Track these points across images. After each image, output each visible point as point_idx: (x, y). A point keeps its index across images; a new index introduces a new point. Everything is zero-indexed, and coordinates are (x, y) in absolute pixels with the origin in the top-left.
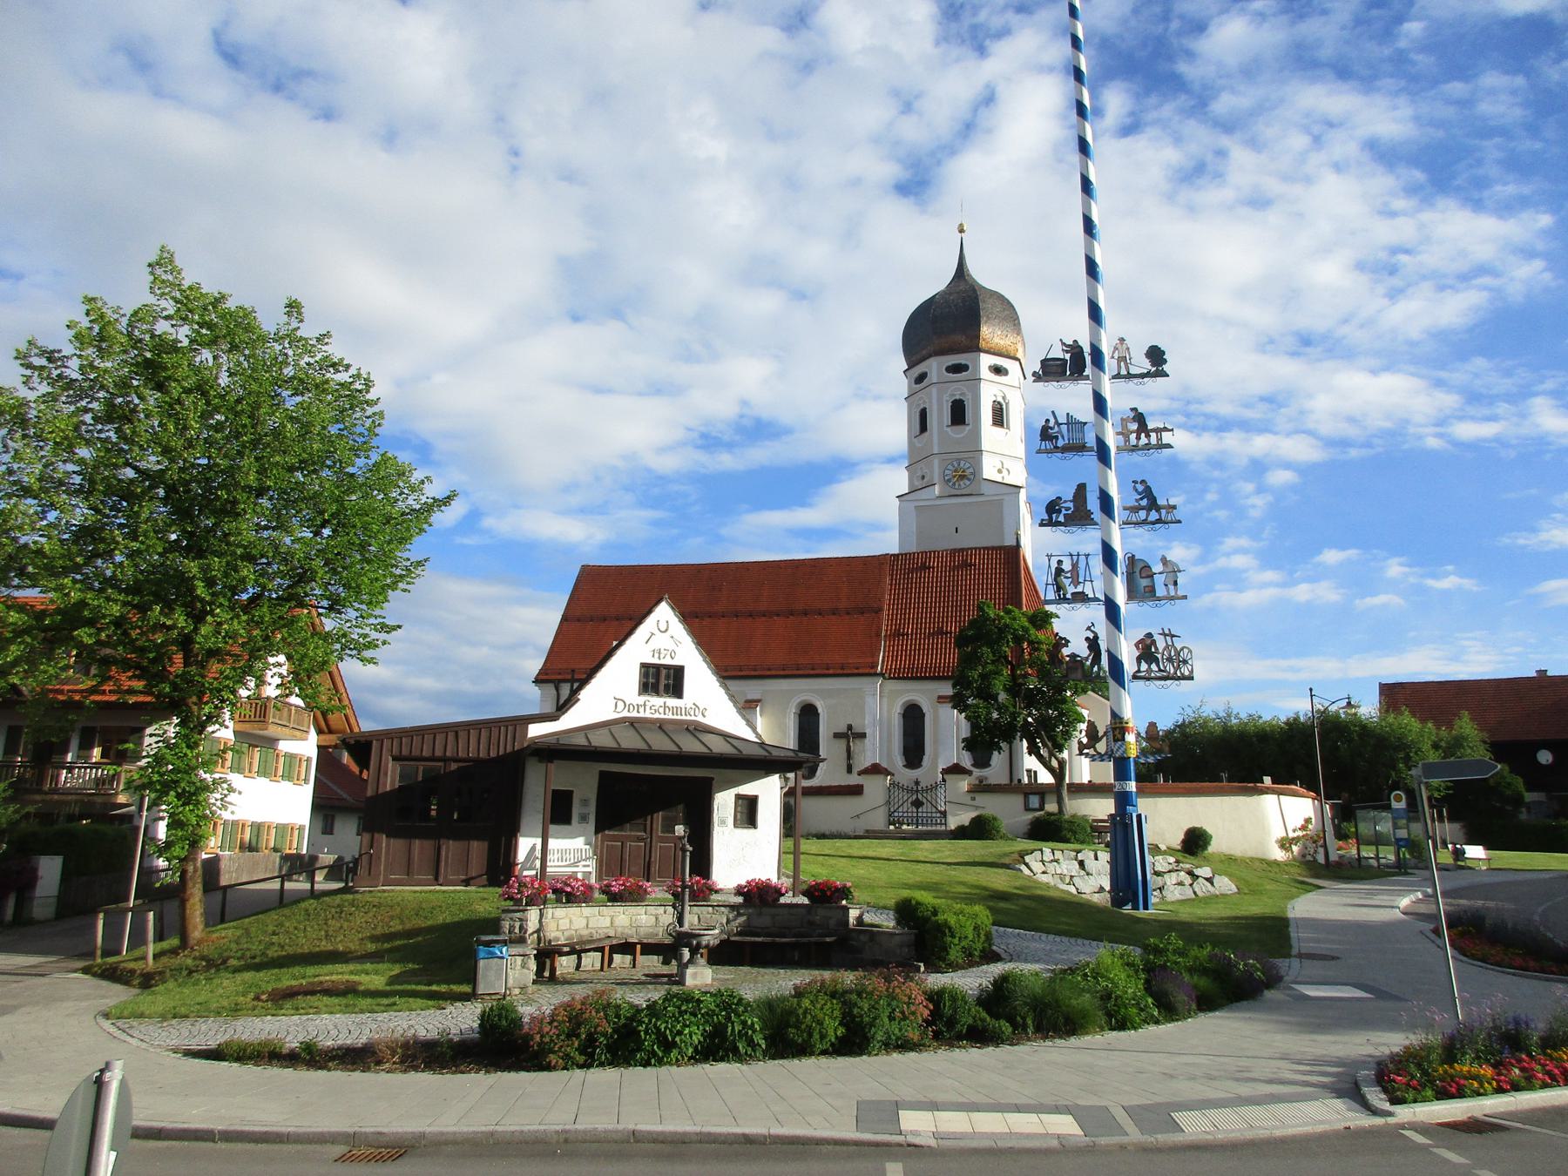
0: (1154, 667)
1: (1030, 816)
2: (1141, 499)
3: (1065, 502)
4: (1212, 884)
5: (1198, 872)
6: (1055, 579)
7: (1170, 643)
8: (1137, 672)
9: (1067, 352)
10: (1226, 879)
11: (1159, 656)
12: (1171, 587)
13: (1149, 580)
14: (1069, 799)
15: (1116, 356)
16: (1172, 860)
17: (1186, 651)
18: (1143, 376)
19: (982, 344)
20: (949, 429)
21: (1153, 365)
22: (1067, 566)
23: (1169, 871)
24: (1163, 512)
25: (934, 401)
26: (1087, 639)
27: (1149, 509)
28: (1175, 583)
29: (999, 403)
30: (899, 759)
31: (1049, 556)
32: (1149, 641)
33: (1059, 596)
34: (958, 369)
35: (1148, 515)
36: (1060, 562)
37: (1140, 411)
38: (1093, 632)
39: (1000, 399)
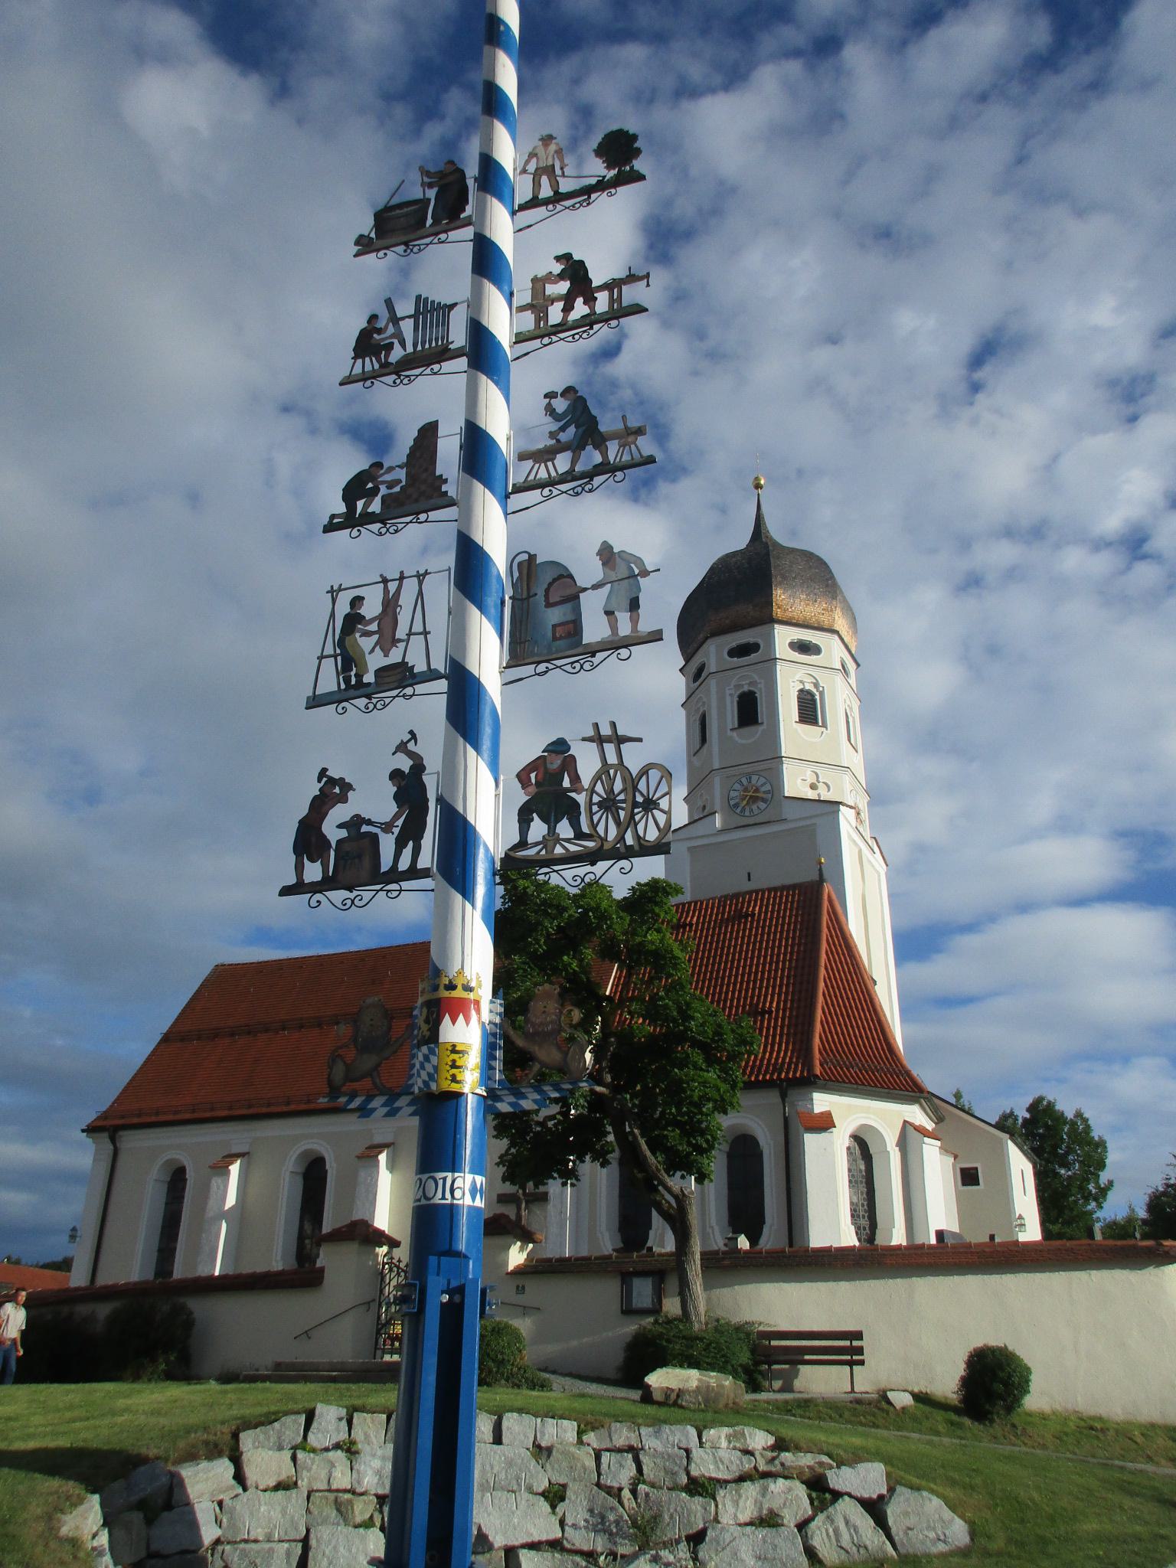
0: (564, 829)
1: (630, 1328)
2: (563, 429)
3: (391, 469)
4: (881, 1522)
5: (840, 1479)
6: (341, 643)
7: (612, 759)
8: (515, 848)
9: (430, 186)
10: (934, 1505)
11: (581, 798)
12: (624, 619)
13: (568, 606)
14: (708, 1286)
15: (532, 167)
16: (760, 1439)
17: (654, 775)
18: (587, 191)
19: (777, 613)
20: (734, 734)
21: (609, 168)
22: (371, 608)
23: (742, 1479)
24: (613, 448)
25: (714, 704)
26: (396, 775)
27: (576, 447)
28: (634, 605)
29: (809, 693)
30: (607, 1235)
31: (334, 593)
32: (556, 763)
33: (347, 680)
34: (744, 650)
35: (574, 462)
36: (357, 601)
37: (576, 257)
38: (411, 755)
39: (809, 687)
